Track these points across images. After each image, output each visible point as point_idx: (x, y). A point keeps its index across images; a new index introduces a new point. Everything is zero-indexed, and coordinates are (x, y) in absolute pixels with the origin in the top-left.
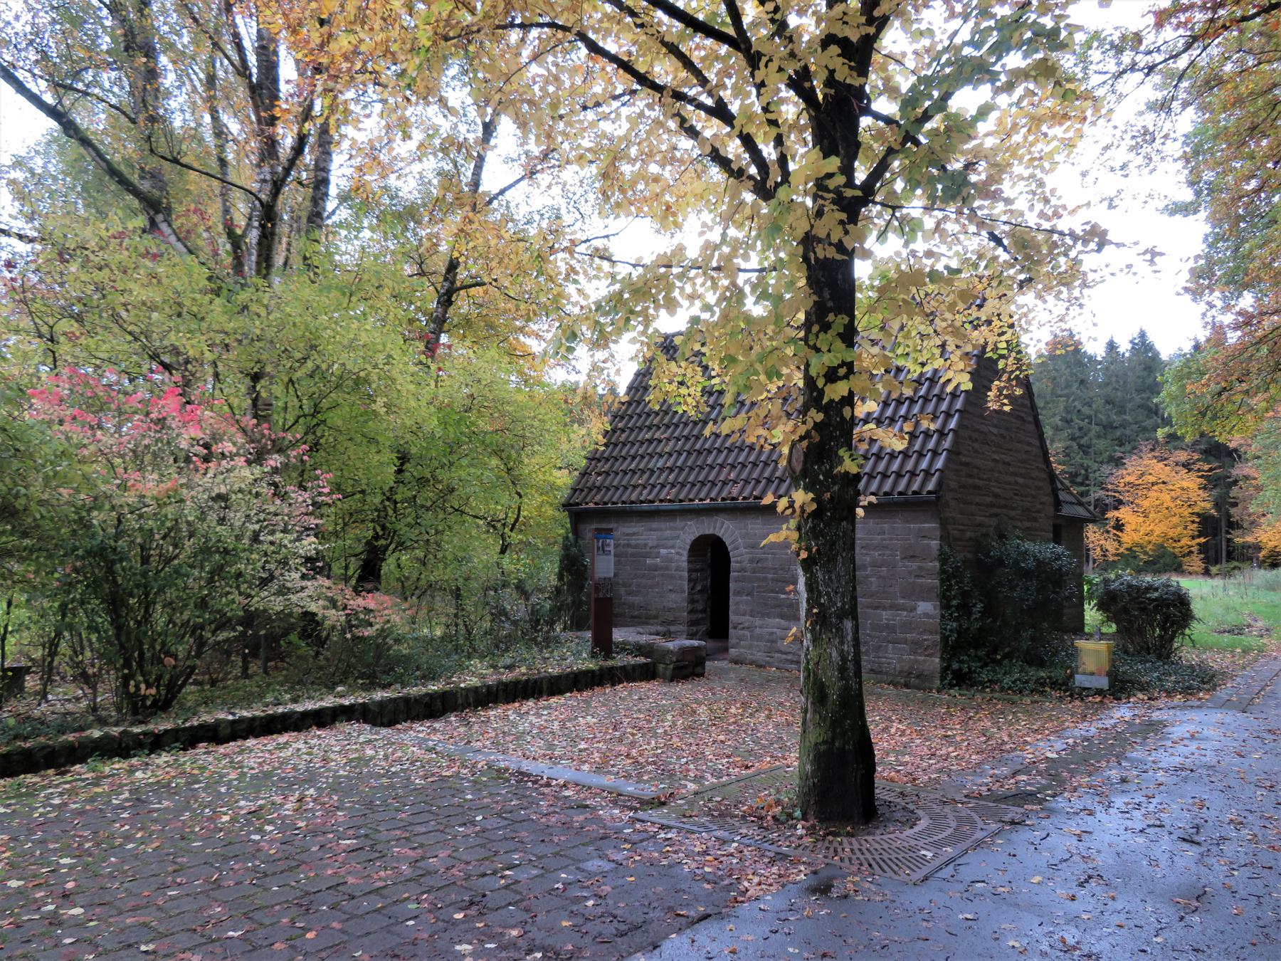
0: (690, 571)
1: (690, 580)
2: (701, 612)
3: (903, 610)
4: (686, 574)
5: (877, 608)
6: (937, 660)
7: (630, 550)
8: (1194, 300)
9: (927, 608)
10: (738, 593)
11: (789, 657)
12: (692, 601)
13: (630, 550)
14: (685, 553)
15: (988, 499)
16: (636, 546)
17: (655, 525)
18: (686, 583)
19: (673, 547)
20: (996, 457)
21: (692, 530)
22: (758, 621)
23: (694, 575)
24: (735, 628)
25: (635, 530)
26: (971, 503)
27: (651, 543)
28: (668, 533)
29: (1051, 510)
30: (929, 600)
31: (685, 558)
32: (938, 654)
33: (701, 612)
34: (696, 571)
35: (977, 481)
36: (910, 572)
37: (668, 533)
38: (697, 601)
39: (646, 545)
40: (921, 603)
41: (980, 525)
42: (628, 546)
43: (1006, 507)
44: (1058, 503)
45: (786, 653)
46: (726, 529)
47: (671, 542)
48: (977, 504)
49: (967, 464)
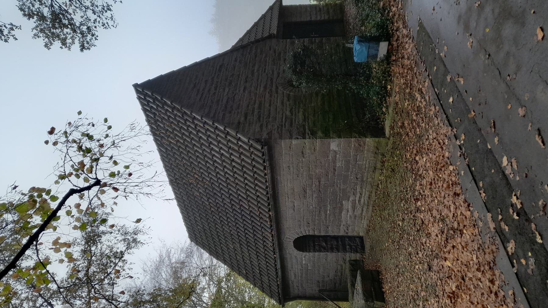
0: (315, 251)
1: (320, 251)
2: (337, 242)
3: (336, 157)
4: (317, 254)
5: (335, 169)
6: (367, 139)
7: (304, 275)
8: (29, 19)
9: (334, 144)
10: (327, 232)
11: (365, 209)
12: (332, 250)
13: (304, 275)
14: (304, 254)
15: (267, 95)
16: (302, 274)
17: (289, 266)
18: (322, 253)
19: (302, 259)
20: (242, 89)
21: (291, 251)
22: (344, 223)
23: (317, 248)
24: (347, 233)
25: (292, 274)
26: (270, 110)
27: (300, 267)
28: (294, 261)
29: (274, 41)
30: (329, 144)
31: (308, 254)
32: (364, 139)
33: (337, 242)
34: (314, 247)
35: (256, 106)
36: (312, 154)
37: (294, 261)
38: (332, 245)
39: (301, 270)
40: (331, 148)
41: (282, 103)
42: (301, 277)
43: (272, 79)
44: (270, 37)
45: (362, 210)
46: (291, 234)
47: (299, 259)
48: (270, 106)
49: (246, 116)
